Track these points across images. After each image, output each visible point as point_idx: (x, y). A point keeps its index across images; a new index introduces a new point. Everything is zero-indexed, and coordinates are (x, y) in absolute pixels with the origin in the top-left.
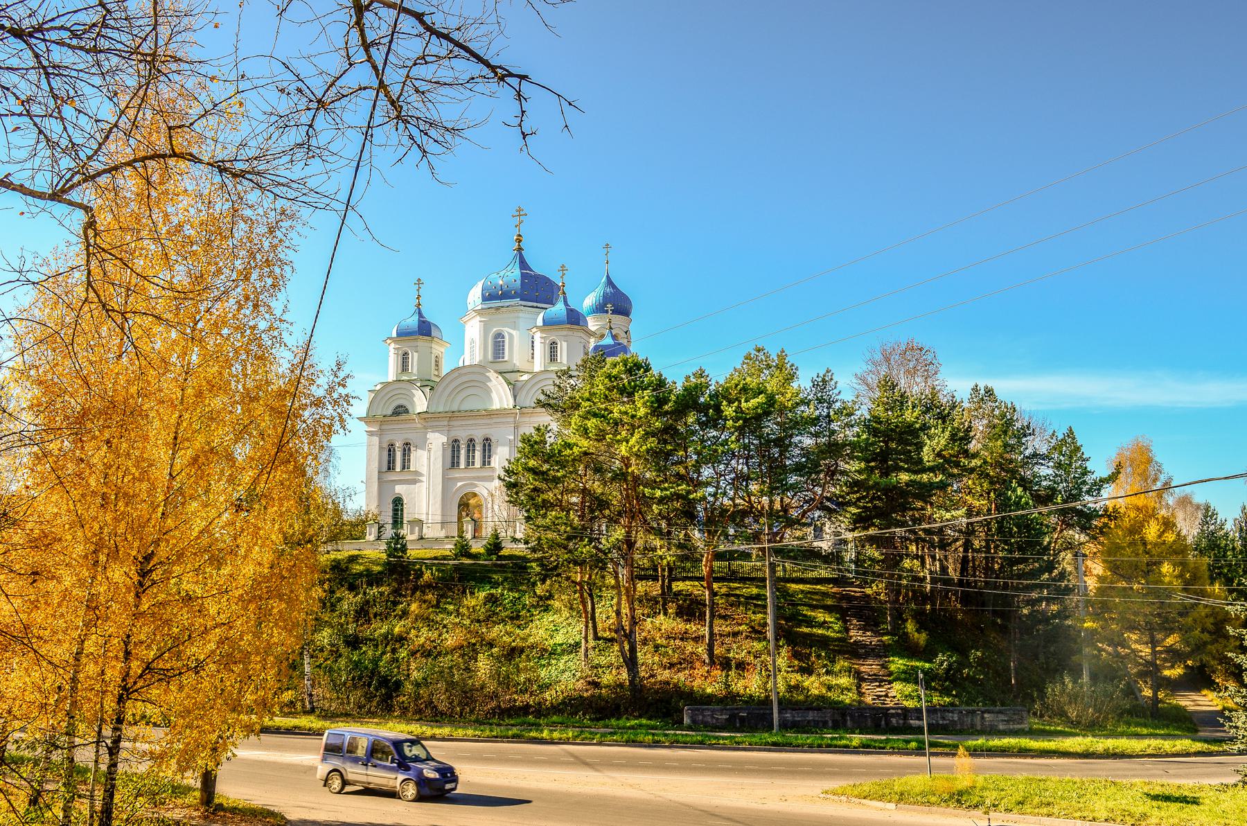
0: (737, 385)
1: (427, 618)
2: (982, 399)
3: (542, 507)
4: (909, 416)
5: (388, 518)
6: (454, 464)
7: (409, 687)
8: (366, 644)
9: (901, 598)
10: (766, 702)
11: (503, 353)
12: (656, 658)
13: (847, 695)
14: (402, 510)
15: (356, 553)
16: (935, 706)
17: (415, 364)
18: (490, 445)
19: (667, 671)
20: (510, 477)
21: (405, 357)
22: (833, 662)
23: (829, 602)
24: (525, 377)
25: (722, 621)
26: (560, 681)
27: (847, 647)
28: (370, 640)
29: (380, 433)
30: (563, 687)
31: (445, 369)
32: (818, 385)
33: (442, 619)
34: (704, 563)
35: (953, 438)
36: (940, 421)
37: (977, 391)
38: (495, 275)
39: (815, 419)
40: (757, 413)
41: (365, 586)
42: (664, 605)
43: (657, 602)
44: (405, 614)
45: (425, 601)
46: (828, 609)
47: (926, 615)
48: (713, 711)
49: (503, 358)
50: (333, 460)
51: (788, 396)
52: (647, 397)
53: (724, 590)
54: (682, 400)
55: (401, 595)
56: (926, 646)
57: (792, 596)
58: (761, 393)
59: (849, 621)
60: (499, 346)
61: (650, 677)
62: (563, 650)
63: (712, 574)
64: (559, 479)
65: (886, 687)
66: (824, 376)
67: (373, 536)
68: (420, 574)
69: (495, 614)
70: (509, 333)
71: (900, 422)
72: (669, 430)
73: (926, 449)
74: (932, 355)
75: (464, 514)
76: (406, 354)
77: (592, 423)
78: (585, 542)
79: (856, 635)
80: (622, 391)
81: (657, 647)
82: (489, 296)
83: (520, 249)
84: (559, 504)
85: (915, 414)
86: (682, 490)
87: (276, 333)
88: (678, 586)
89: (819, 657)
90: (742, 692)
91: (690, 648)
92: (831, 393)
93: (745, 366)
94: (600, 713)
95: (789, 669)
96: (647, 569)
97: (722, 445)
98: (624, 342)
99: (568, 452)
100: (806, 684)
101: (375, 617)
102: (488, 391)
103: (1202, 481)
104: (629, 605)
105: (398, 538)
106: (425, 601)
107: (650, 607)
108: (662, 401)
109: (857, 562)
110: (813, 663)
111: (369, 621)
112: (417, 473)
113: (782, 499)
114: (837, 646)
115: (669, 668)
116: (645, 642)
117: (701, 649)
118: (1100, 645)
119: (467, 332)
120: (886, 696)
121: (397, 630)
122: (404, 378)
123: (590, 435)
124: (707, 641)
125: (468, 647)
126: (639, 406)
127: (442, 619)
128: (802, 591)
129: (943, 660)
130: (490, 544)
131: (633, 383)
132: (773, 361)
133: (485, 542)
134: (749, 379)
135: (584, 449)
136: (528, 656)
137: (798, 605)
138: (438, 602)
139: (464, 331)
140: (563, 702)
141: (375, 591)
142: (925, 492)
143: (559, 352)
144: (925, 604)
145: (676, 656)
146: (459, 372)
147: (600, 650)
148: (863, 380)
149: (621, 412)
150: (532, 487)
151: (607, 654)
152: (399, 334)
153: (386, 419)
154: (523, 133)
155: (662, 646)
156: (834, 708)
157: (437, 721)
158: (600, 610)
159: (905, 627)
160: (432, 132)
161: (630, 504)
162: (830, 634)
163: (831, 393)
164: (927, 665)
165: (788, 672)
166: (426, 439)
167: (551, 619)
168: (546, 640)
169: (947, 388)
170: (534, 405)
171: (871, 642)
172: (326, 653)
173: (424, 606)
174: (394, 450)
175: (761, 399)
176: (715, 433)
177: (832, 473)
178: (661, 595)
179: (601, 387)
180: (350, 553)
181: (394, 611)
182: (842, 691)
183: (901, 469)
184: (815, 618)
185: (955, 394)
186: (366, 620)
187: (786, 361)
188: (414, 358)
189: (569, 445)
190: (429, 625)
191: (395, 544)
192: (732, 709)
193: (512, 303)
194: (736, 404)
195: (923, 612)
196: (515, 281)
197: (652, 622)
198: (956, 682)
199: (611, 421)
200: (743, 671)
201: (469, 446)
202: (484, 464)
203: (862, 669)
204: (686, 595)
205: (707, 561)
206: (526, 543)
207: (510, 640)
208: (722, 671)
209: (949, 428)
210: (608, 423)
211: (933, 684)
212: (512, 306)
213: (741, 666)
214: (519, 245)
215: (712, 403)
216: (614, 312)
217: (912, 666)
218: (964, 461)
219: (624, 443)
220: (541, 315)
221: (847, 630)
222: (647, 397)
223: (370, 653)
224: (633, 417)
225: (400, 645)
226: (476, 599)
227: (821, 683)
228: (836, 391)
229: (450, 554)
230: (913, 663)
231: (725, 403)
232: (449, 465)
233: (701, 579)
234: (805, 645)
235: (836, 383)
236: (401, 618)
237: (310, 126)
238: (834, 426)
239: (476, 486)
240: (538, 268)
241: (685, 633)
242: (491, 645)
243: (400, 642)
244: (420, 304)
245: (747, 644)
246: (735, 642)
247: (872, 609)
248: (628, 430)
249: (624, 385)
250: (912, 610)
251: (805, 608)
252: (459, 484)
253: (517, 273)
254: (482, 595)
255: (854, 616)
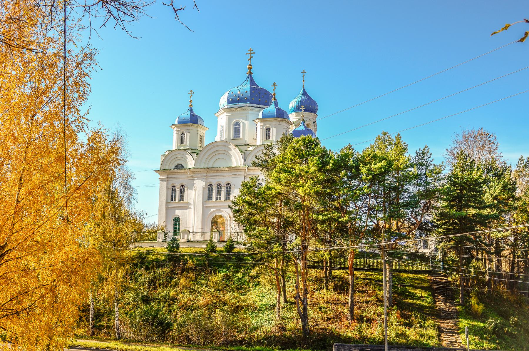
1: (189, 287)
2: (525, 165)
3: (253, 224)
4: (475, 175)
5: (170, 228)
6: (209, 198)
7: (175, 326)
8: (154, 301)
9: (469, 284)
10: (382, 343)
11: (239, 134)
12: (320, 315)
13: (432, 340)
14: (179, 225)
15: (151, 248)
16: (485, 349)
18: (230, 188)
19: (326, 322)
20: (235, 206)
21: (182, 136)
22: (425, 320)
23: (425, 285)
24: (251, 148)
25: (360, 294)
26: (263, 326)
27: (434, 312)
28: (156, 299)
29: (167, 180)
30: (265, 330)
31: (206, 143)
32: (419, 155)
33: (198, 288)
34: (348, 259)
35: (504, 187)
36: (496, 178)
37: (522, 160)
38: (235, 89)
39: (417, 175)
41: (155, 268)
42: (327, 283)
43: (323, 282)
44: (177, 284)
45: (188, 278)
46: (425, 289)
47: (485, 294)
48: (351, 347)
49: (239, 137)
50: (133, 194)
51: (401, 161)
52: (315, 161)
53: (363, 276)
54: (337, 163)
55: (175, 274)
56: (483, 313)
57: (403, 280)
58: (384, 159)
59: (437, 296)
60: (237, 130)
61: (315, 325)
62: (266, 308)
64: (263, 208)
65: (456, 336)
66: (424, 150)
67: (161, 239)
68: (186, 262)
69: (228, 286)
70: (243, 123)
71: (469, 179)
72: (330, 181)
73: (486, 195)
74: (494, 138)
75: (214, 227)
76: (183, 134)
77: (283, 176)
78: (277, 245)
79: (440, 305)
80: (301, 157)
81: (321, 308)
82: (231, 101)
83: (250, 73)
85: (479, 174)
86: (335, 216)
88: (335, 273)
89: (416, 317)
90: (369, 336)
91: (340, 309)
92: (427, 160)
93: (377, 143)
94: (284, 345)
95: (397, 324)
97: (360, 190)
98: (312, 129)
99: (269, 192)
100: (408, 333)
101: (160, 286)
102: (229, 156)
104: (303, 283)
105: (174, 240)
106: (188, 278)
107: (318, 285)
108: (324, 164)
109: (443, 261)
110: (412, 321)
111: (156, 288)
112: (188, 203)
114: (428, 311)
115: (327, 321)
116: (313, 305)
117: (347, 310)
119: (219, 122)
120: (456, 342)
121: (171, 294)
124: (350, 305)
125: (211, 305)
126: (311, 166)
127: (198, 288)
128: (409, 278)
129: (492, 322)
130: (227, 246)
131: (307, 153)
132: (393, 140)
133: (224, 244)
134: (377, 151)
136: (245, 311)
137: (406, 286)
138: (196, 278)
139: (217, 121)
140: (264, 339)
141: (160, 271)
142: (484, 221)
143: (271, 136)
144: (484, 288)
145: (332, 313)
146: (213, 145)
147: (287, 309)
148: (452, 153)
149: (299, 170)
150: (248, 212)
151: (291, 311)
152: (179, 123)
153: (171, 172)
154: (174, 9)
155: (324, 308)
156: (423, 348)
157: (189, 347)
158: (289, 285)
159: (470, 301)
160: (122, 8)
161: (305, 223)
162: (424, 303)
163: (427, 160)
164: (482, 325)
165: (397, 325)
166: (193, 184)
167: (260, 290)
168: (257, 302)
169: (502, 158)
170: (251, 165)
171: (449, 310)
172: (131, 306)
173: (188, 280)
174: (175, 189)
175: (384, 163)
177: (427, 208)
178: (325, 278)
179: (289, 155)
180: (148, 249)
181: (170, 283)
182: (429, 338)
183: (470, 206)
184: (416, 294)
185: (506, 162)
186: (154, 287)
187: (401, 141)
188: (187, 136)
190: (190, 292)
191: (173, 244)
192: (362, 346)
194: (368, 166)
195: (483, 293)
196: (247, 92)
197: (319, 294)
198: (499, 335)
199: (294, 175)
200: (370, 324)
202: (227, 199)
203: (443, 325)
204: (340, 278)
205: (350, 258)
207: (236, 301)
208: (358, 323)
209: (502, 183)
211: (485, 336)
212: (246, 107)
213: (369, 321)
214: (250, 71)
215: (354, 165)
216: (306, 111)
217: (472, 325)
218: (511, 202)
219: (301, 188)
220: (261, 112)
221: (435, 302)
222: (315, 161)
223: (155, 307)
224: (307, 172)
225: (173, 302)
226: (218, 277)
227: (416, 333)
228: (431, 159)
229: (204, 250)
230: (474, 323)
231: (362, 165)
232: (206, 199)
233: (347, 268)
234: (409, 310)
235: (431, 154)
236: (174, 287)
237: (52, 6)
238: (429, 180)
239: (222, 211)
241: (338, 300)
242: (225, 304)
243: (173, 300)
244: (191, 105)
245: (373, 308)
246: (367, 307)
247: (452, 290)
248: (305, 180)
250: (476, 291)
251: (410, 288)
252: (212, 210)
253: (248, 87)
254: (221, 275)
255: (440, 293)
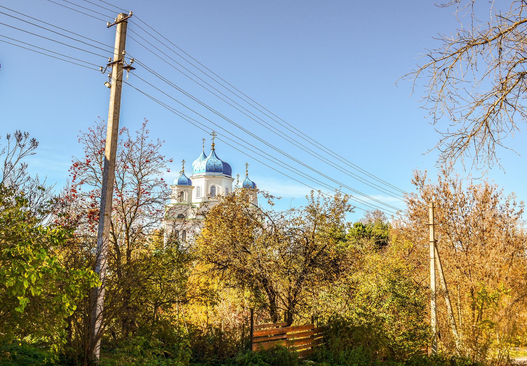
70: (218, 187)
103: (310, 168)
118: (292, 339)
152: (179, 184)
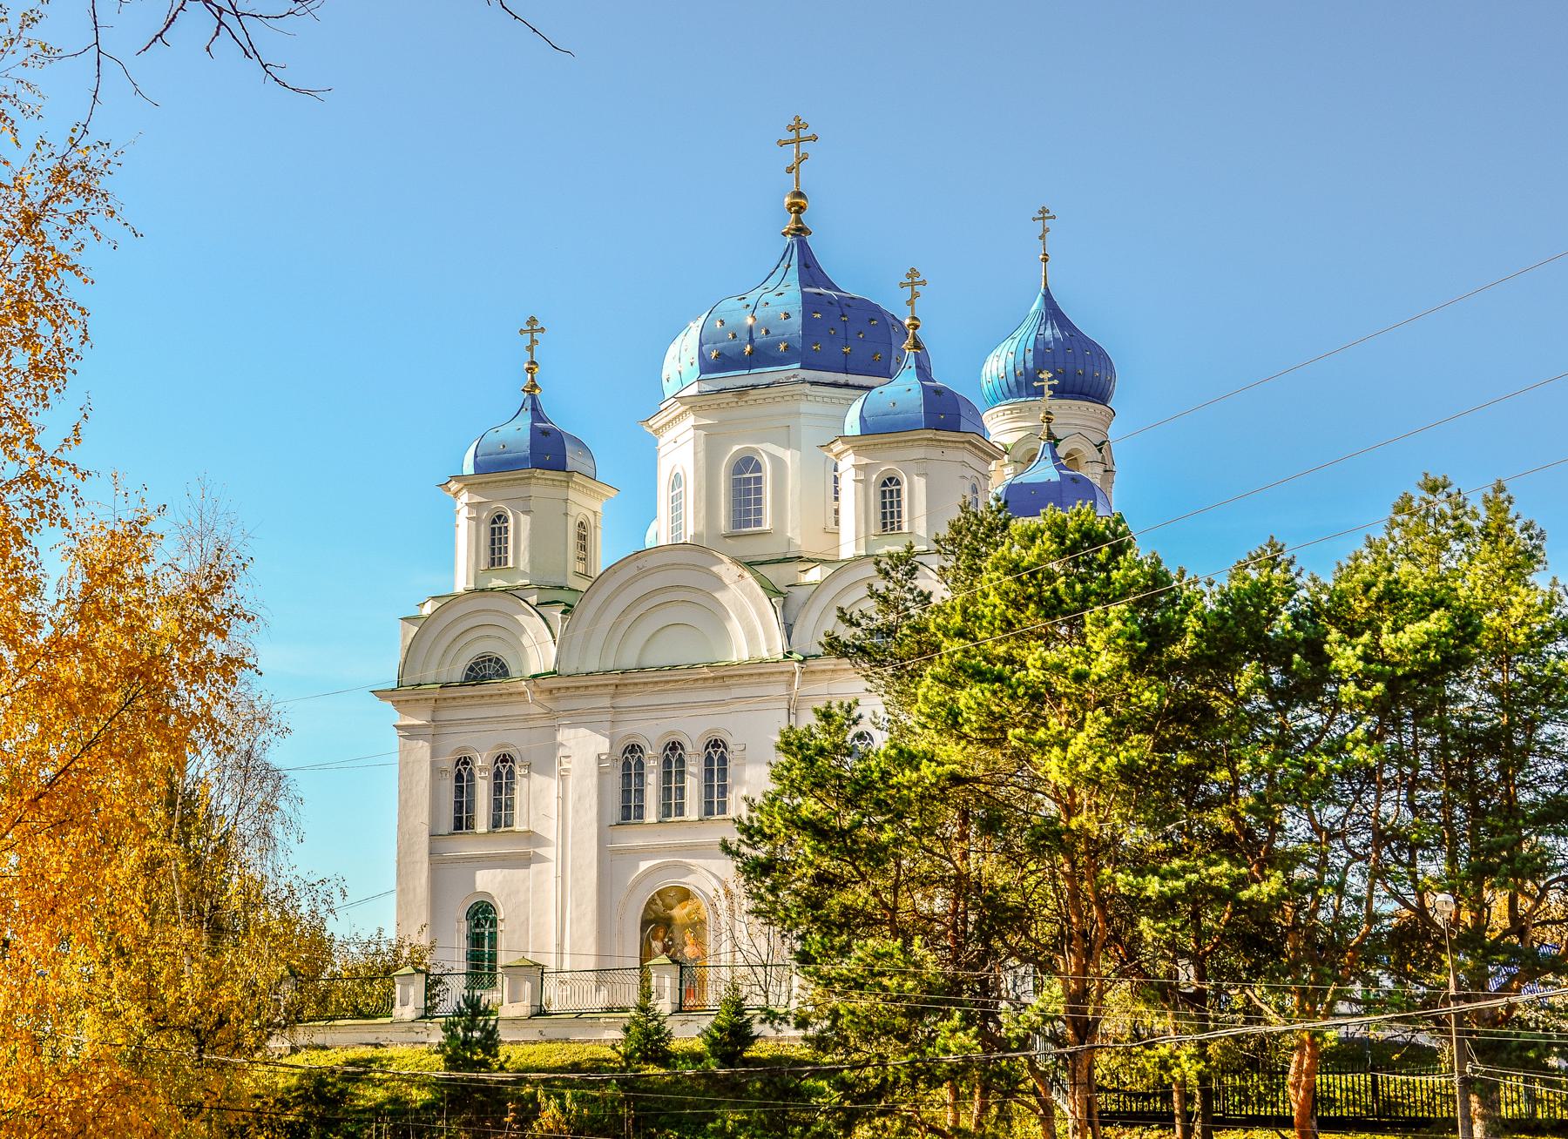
0: (1368, 587)
3: (841, 927)
5: (455, 957)
6: (630, 811)
11: (759, 512)
14: (493, 937)
15: (367, 1052)
17: (524, 544)
18: (723, 760)
20: (753, 846)
24: (815, 575)
29: (434, 732)
31: (604, 556)
34: (1291, 1079)
38: (733, 303)
40: (1424, 662)
49: (758, 523)
50: (282, 804)
51: (1516, 612)
52: (1117, 625)
54: (1218, 630)
63: (1315, 1108)
64: (884, 848)
67: (411, 1007)
70: (773, 457)
75: (657, 945)
76: (500, 518)
77: (968, 697)
80: (1052, 608)
82: (717, 361)
83: (800, 231)
84: (887, 919)
87: (41, 493)
93: (1396, 532)
96: (1146, 1097)
97: (1329, 752)
98: (1093, 474)
99: (909, 775)
102: (717, 615)
105: (474, 1010)
112: (531, 837)
113: (1513, 902)
122: (496, 583)
123: (966, 729)
126: (1096, 647)
130: (720, 1029)
131: (1078, 587)
133: (706, 1023)
134: (1403, 569)
135: (948, 768)
143: (905, 504)
146: (640, 563)
150: (811, 872)
153: (449, 693)
161: (1079, 915)
174: (471, 774)
175: (1438, 622)
176: (1315, 720)
179: (994, 598)
180: (351, 1054)
187: (1511, 516)
188: (520, 528)
189: (912, 757)
191: (467, 1029)
193: (781, 376)
194: (1366, 637)
196: (787, 316)
199: (1021, 691)
201: (667, 762)
202: (709, 812)
205: (1299, 1072)
206: (803, 1023)
210: (1013, 697)
215: (1300, 635)
216: (1060, 392)
219: (1056, 750)
222: (1117, 625)
224: (1080, 677)
229: (614, 1055)
231: (1334, 635)
239: (688, 870)
240: (850, 281)
244: (534, 386)
249: (1055, 591)
252: (644, 866)
